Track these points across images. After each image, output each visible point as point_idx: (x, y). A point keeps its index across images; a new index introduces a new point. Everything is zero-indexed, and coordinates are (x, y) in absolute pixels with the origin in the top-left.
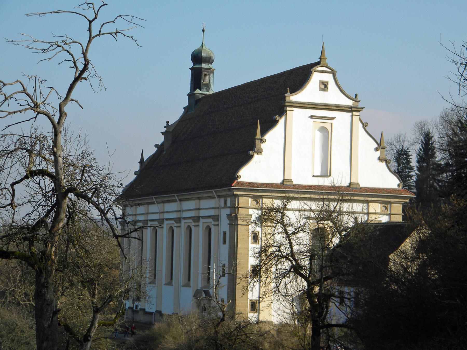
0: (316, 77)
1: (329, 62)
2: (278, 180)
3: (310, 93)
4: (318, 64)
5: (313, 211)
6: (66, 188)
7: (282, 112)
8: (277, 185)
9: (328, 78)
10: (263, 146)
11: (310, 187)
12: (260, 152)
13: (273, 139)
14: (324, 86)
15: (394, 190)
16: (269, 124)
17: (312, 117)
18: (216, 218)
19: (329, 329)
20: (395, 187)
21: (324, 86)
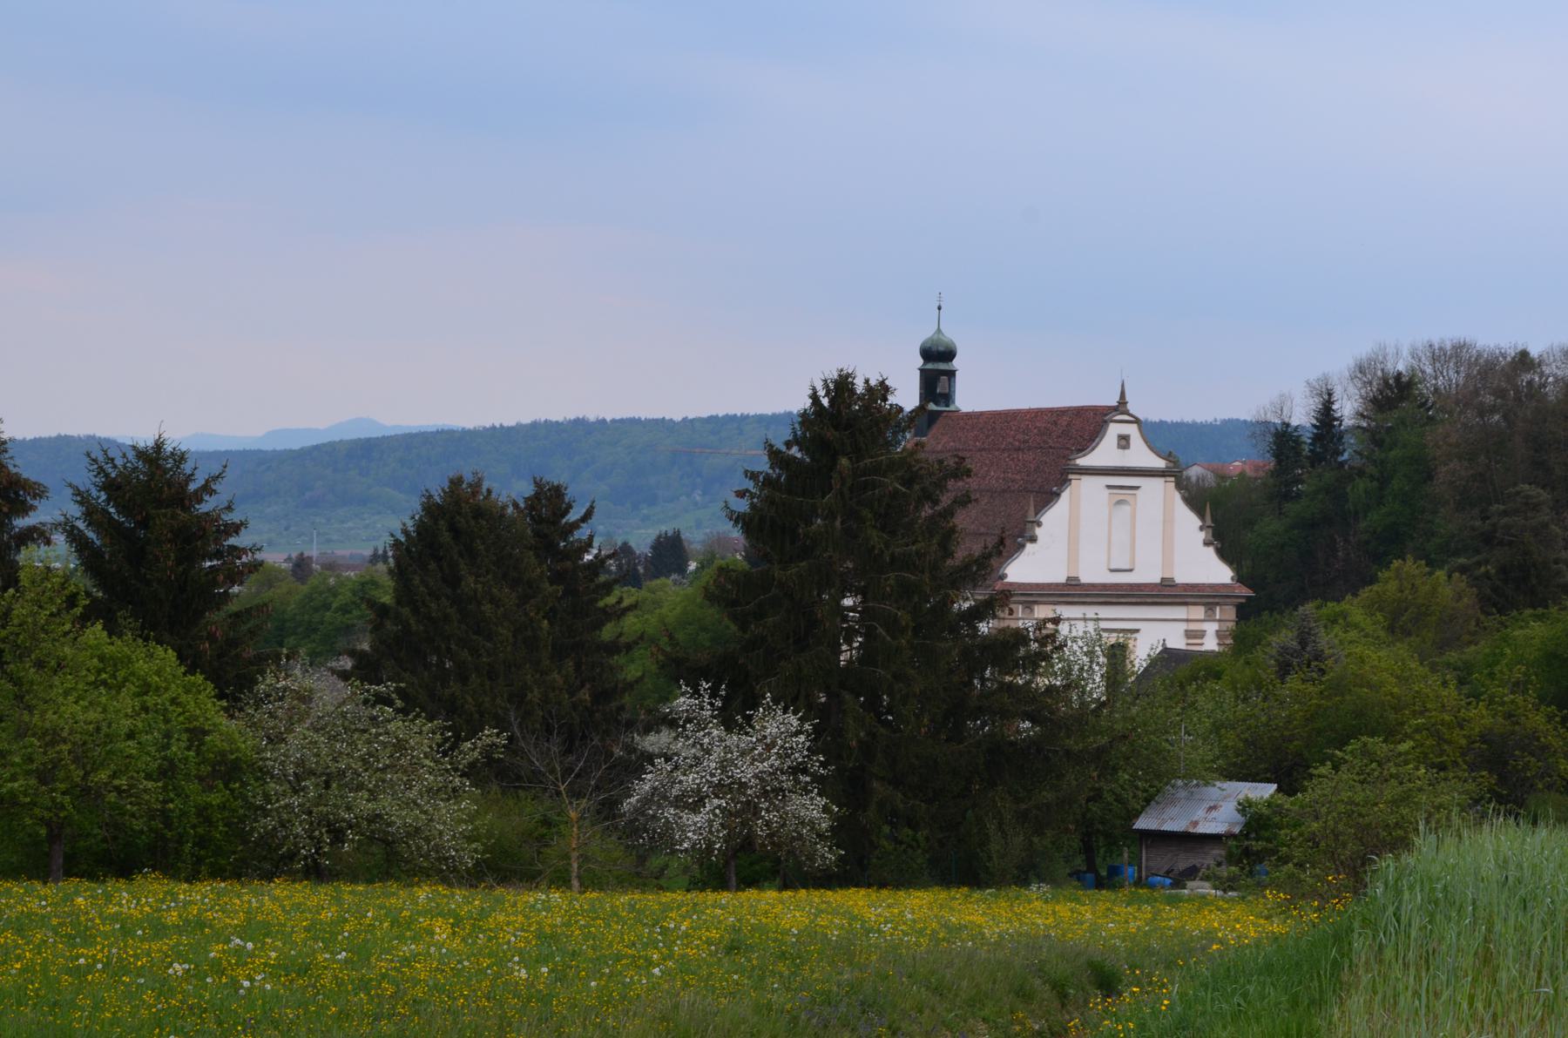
0: (1114, 430)
1: (1130, 407)
2: (1061, 578)
3: (1104, 453)
4: (1115, 409)
5: (115, 467)
6: (1354, 607)
7: (1064, 482)
8: (1057, 585)
9: (1132, 430)
10: (1038, 531)
11: (1105, 586)
12: (1033, 539)
13: (1054, 520)
14: (1124, 441)
15: (1224, 586)
16: (1048, 497)
17: (1109, 487)
18: (708, 752)
19: (906, 396)
20: (1228, 581)
21: (1124, 441)
